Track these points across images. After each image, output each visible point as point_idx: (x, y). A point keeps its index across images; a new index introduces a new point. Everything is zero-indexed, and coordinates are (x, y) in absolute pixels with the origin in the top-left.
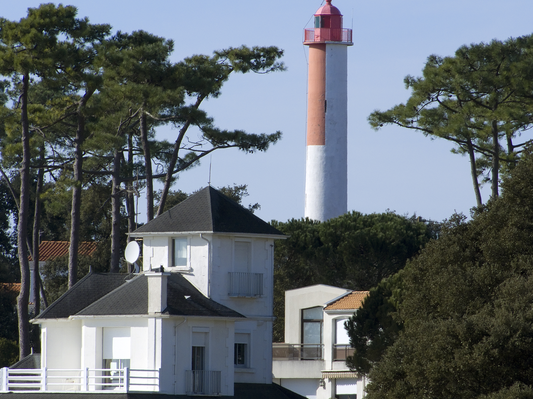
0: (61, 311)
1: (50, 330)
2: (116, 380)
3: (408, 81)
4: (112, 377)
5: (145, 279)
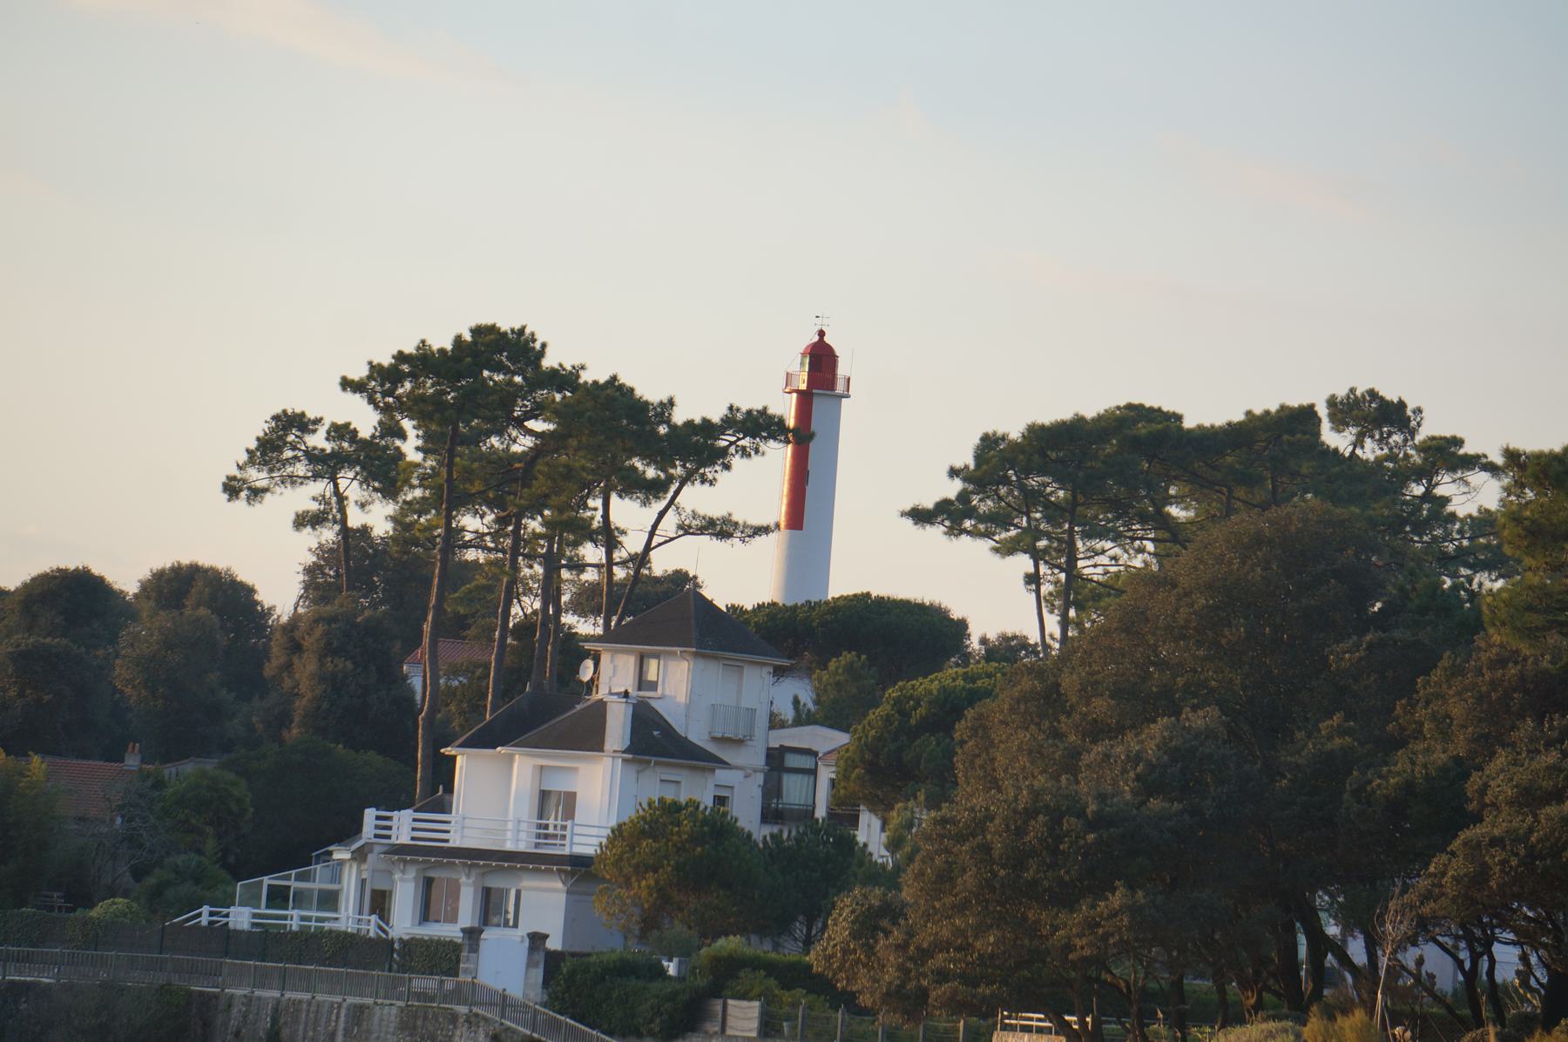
0: (486, 739)
1: (468, 766)
2: (555, 836)
3: (954, 472)
4: (551, 830)
5: (602, 705)
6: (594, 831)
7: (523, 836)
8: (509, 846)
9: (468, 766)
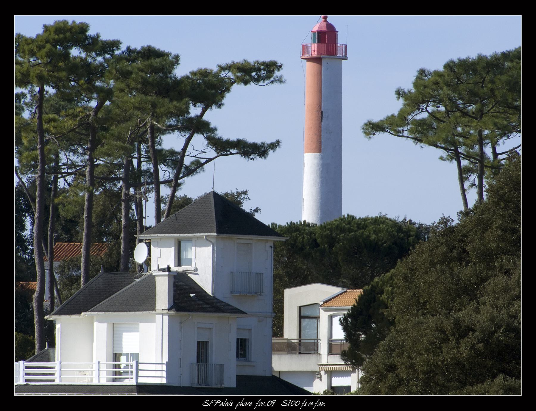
0: (74, 308)
1: (64, 326)
3: (399, 93)
4: (122, 370)
5: (152, 278)
6: (159, 367)
7: (103, 374)
8: (95, 382)
9: (64, 326)
